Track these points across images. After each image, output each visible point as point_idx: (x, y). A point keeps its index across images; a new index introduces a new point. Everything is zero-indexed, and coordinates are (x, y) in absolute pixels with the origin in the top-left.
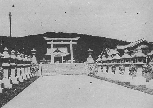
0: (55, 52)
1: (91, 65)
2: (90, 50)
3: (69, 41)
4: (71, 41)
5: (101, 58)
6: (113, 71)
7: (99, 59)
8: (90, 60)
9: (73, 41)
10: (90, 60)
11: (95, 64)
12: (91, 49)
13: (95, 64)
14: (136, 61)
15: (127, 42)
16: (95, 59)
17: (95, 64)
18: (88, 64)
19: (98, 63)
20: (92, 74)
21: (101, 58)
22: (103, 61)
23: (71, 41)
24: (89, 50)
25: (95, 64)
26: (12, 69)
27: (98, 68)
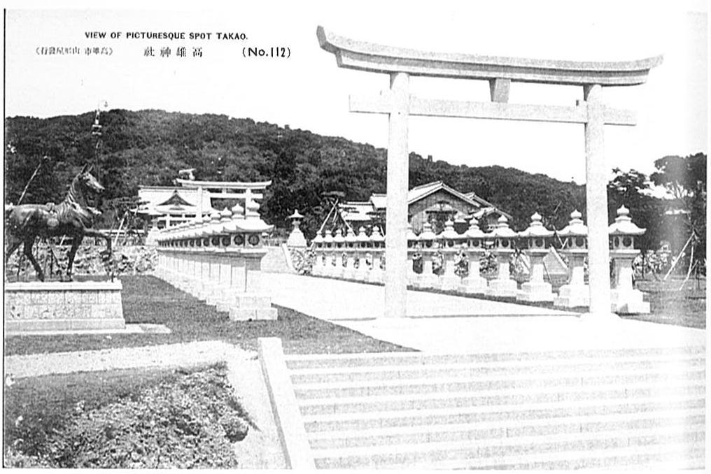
0: (165, 204)
1: (300, 250)
2: (297, 214)
3: (242, 191)
4: (249, 191)
5: (324, 235)
6: (242, 192)
7: (319, 239)
8: (297, 237)
9: (253, 191)
10: (297, 237)
11: (310, 249)
12: (300, 214)
13: (308, 249)
14: (531, 246)
15: (435, 160)
16: (309, 234)
17: (310, 249)
18: (292, 248)
19: (63, 244)
20: (302, 272)
21: (324, 235)
22: (325, 243)
23: (249, 191)
24: (293, 216)
25: (308, 249)
26: (572, 238)
27: (314, 258)
